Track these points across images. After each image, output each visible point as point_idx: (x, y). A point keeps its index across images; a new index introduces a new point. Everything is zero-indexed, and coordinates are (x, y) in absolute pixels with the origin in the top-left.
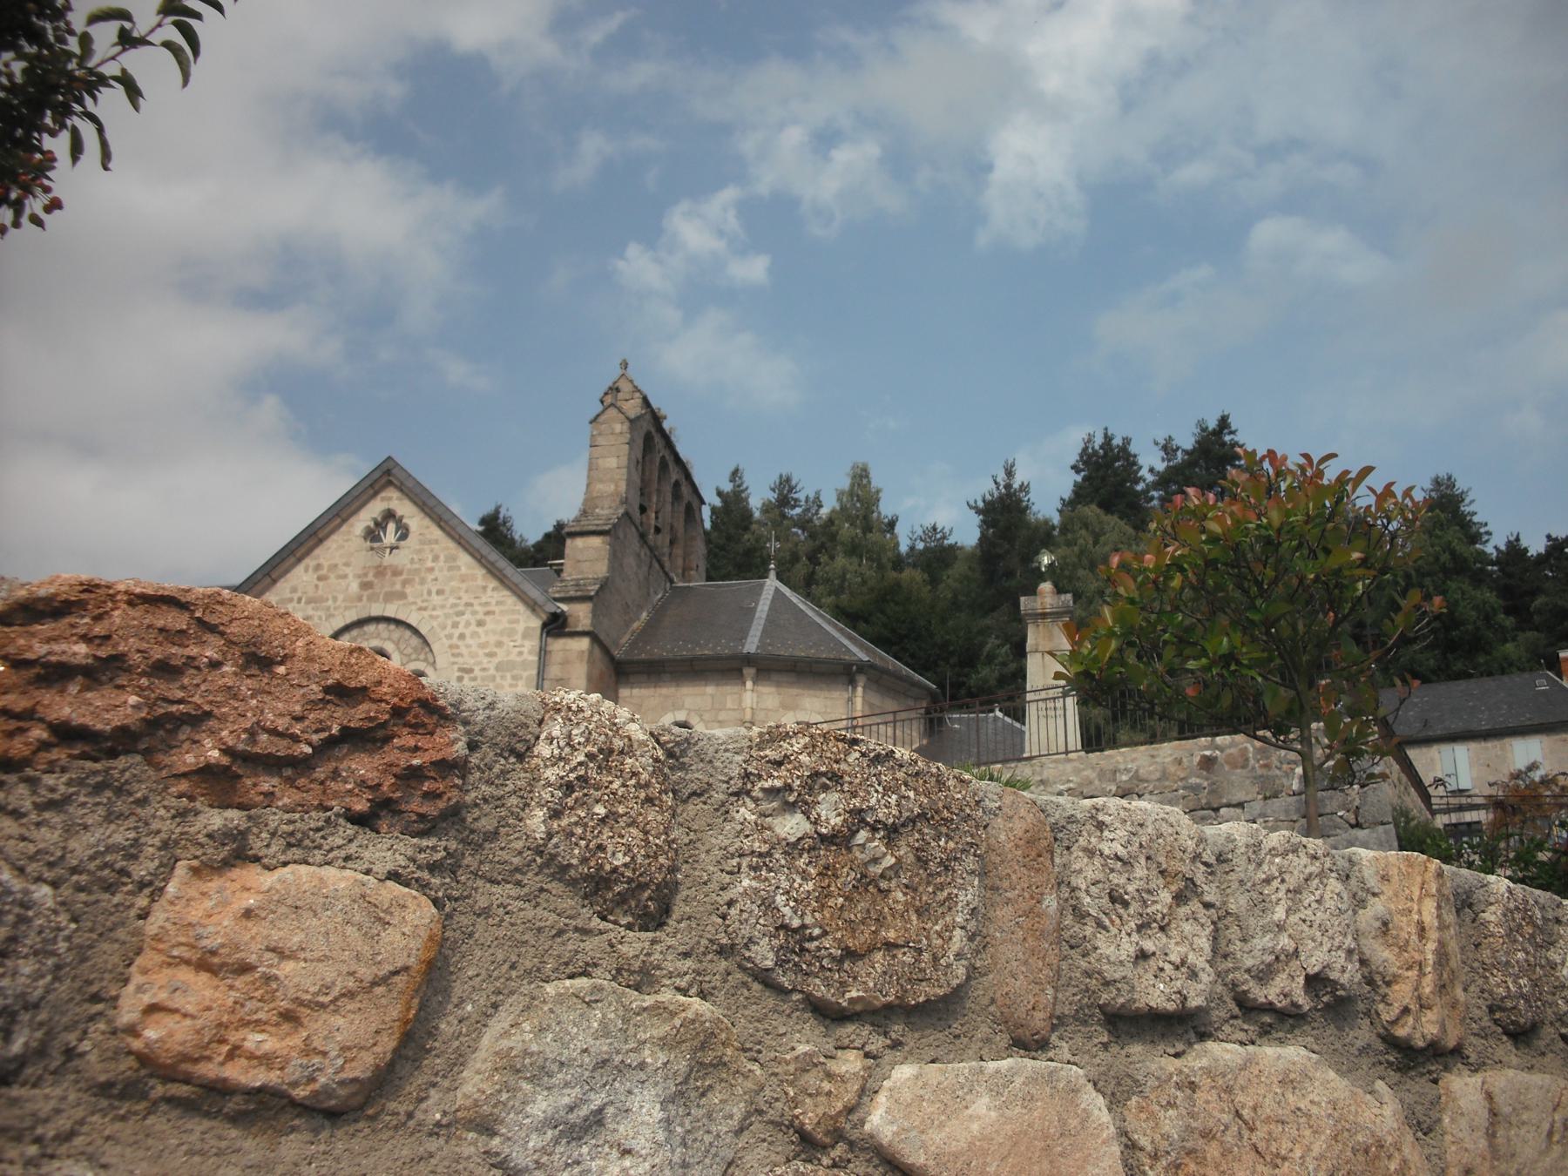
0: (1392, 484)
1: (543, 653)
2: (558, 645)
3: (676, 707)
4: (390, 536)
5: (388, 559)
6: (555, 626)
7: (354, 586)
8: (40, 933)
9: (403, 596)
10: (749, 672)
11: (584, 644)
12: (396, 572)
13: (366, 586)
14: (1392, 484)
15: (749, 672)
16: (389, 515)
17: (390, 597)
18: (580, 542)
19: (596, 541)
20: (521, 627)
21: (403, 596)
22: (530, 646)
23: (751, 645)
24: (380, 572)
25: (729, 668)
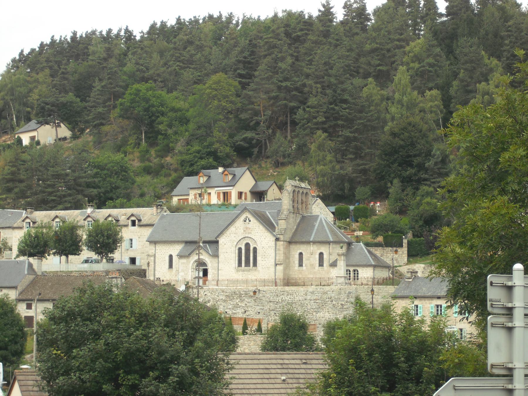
0: (53, 36)
1: (276, 244)
2: (278, 243)
3: (300, 249)
4: (247, 221)
5: (248, 226)
6: (277, 239)
7: (242, 231)
8: (311, 61)
9: (251, 233)
10: (311, 243)
11: (282, 243)
12: (250, 229)
13: (244, 231)
14: (53, 36)
15: (311, 243)
16: (247, 217)
17: (249, 233)
18: (281, 221)
19: (284, 221)
20: (271, 240)
21: (251, 233)
22: (274, 243)
23: (311, 240)
24: (247, 228)
25: (308, 243)
